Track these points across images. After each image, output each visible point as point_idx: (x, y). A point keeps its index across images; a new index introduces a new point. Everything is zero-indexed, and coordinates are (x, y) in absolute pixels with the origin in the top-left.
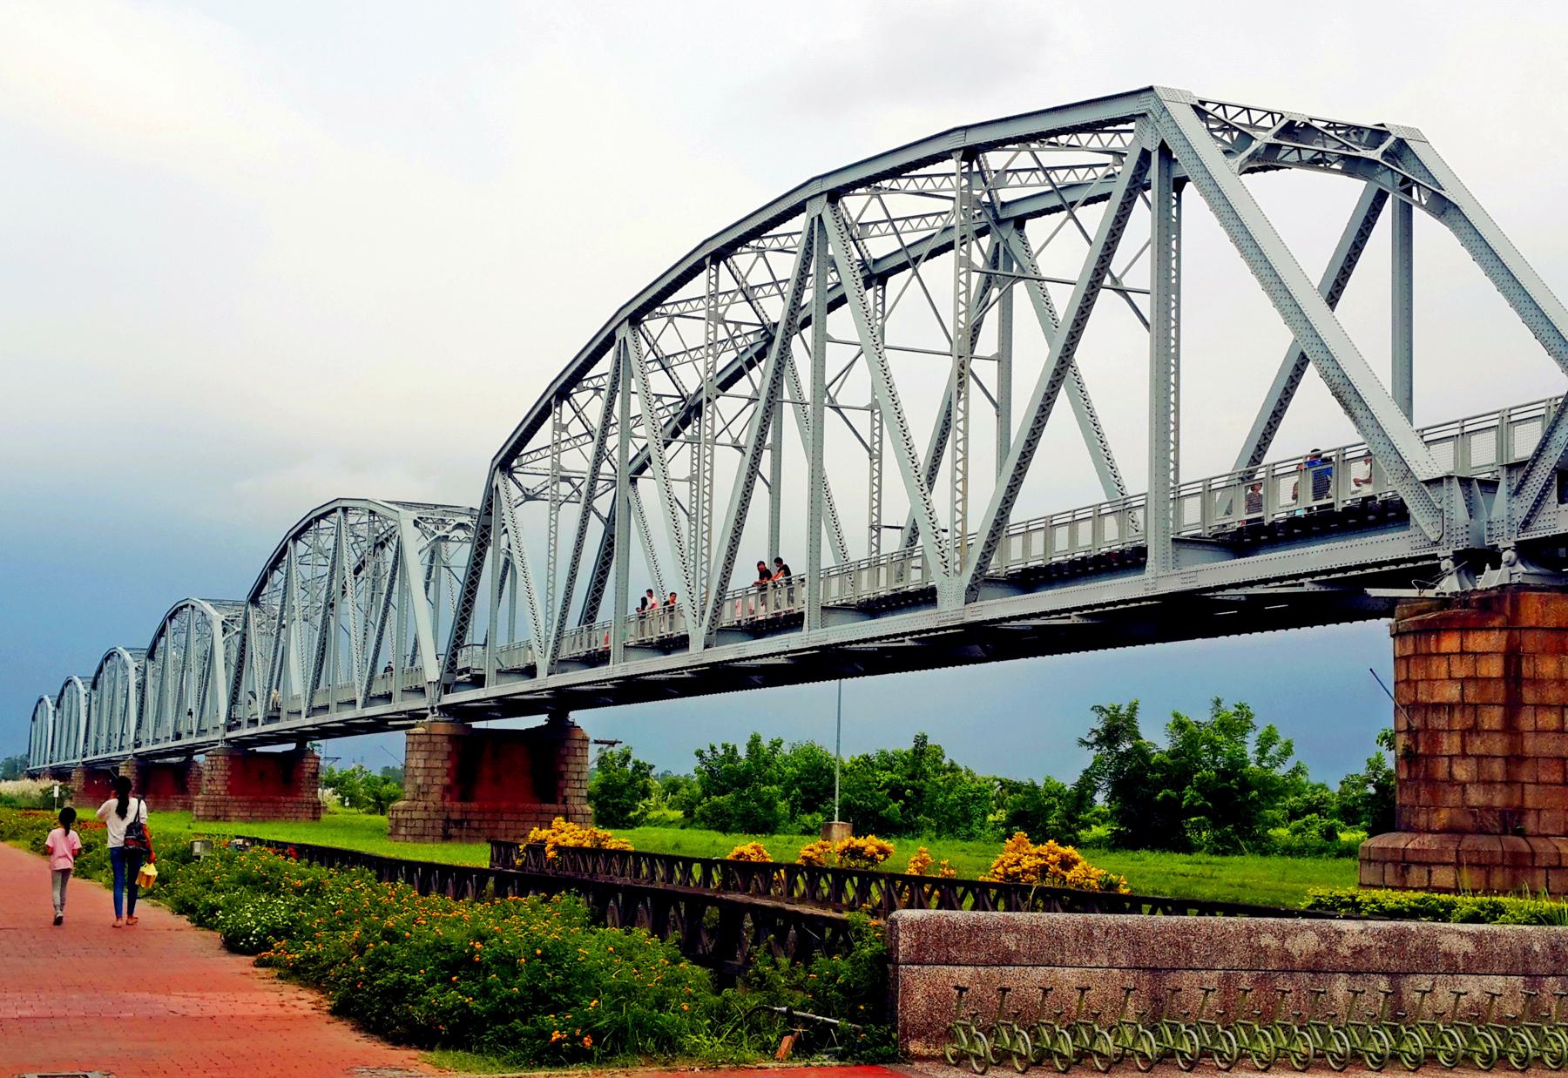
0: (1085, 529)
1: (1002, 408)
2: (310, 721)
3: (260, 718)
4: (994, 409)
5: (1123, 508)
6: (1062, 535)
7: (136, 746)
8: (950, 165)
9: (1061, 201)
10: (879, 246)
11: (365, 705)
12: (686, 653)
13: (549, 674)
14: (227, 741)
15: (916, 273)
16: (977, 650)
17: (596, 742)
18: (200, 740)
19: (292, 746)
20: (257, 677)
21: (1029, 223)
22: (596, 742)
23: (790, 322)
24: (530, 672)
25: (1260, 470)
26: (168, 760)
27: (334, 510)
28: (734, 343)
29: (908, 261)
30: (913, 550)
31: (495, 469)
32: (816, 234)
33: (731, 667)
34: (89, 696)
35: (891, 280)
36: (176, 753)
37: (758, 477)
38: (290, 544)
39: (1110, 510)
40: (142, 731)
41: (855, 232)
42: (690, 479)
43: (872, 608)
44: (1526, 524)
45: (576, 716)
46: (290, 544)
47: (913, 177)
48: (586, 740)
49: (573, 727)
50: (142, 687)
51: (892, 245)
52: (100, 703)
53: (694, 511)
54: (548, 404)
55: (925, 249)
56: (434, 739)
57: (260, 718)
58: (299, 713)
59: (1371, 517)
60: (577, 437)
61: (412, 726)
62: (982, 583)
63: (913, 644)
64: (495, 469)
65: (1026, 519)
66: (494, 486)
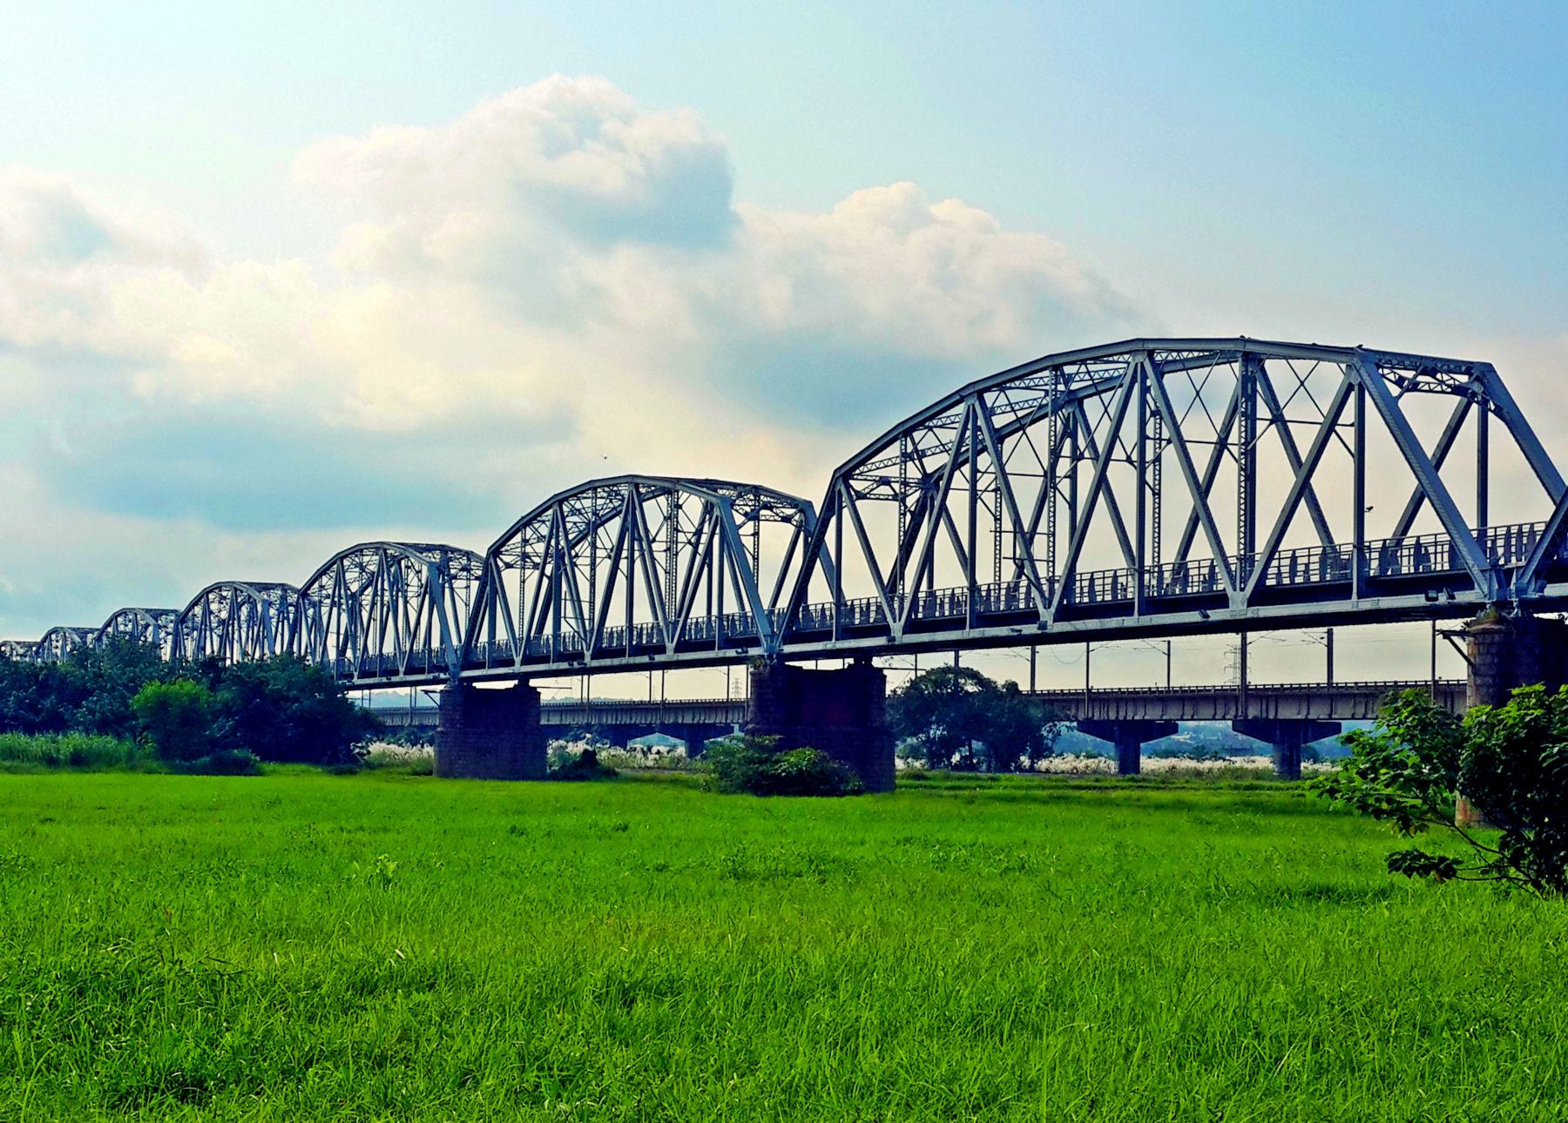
1: (1073, 505)
8: (1046, 373)
9: (1098, 388)
10: (999, 421)
15: (1024, 433)
21: (1085, 401)
23: (953, 464)
28: (1012, 408)
29: (1020, 426)
32: (970, 416)
35: (1007, 440)
37: (1068, 499)
41: (989, 413)
45: (533, 683)
51: (1011, 417)
55: (1029, 420)
59: (1065, 602)
60: (942, 452)
65: (1115, 568)
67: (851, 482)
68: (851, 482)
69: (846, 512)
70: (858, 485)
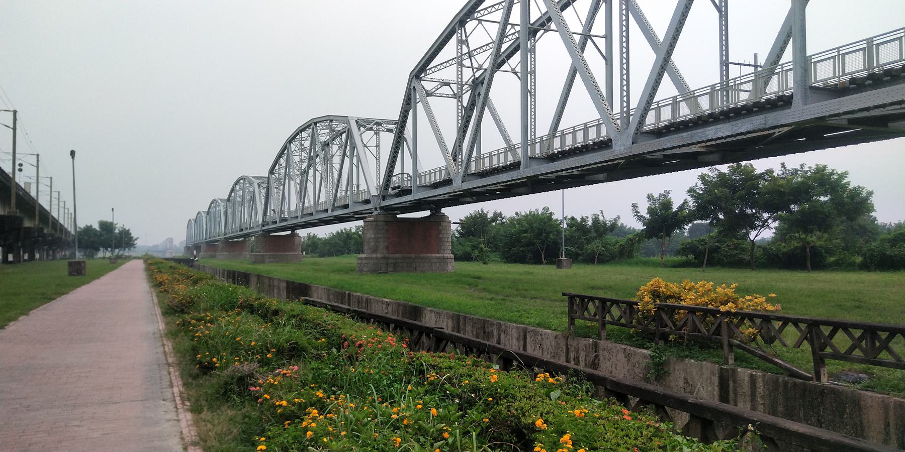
0: (502, 156)
2: (303, 220)
3: (278, 220)
4: (604, 62)
5: (510, 148)
6: (495, 158)
7: (225, 235)
11: (333, 210)
12: (611, 150)
13: (462, 182)
14: (263, 230)
16: (469, 199)
17: (454, 223)
18: (251, 231)
19: (289, 232)
20: (273, 205)
22: (454, 223)
24: (326, 211)
25: (778, 68)
26: (760, 165)
27: (310, 125)
30: (555, 134)
31: (412, 78)
33: (427, 201)
34: (206, 217)
36: (241, 236)
38: (288, 145)
39: (682, 99)
40: (227, 229)
42: (376, 146)
43: (435, 186)
44: (380, 204)
46: (288, 145)
47: (479, 11)
48: (450, 222)
49: (444, 216)
50: (226, 213)
52: (210, 220)
53: (533, 91)
54: (454, 27)
56: (378, 223)
57: (278, 220)
58: (297, 217)
61: (366, 217)
62: (467, 176)
63: (501, 187)
64: (412, 78)
66: (412, 88)
67: (888, 333)
68: (888, 333)
69: (420, 106)
70: (428, 86)
